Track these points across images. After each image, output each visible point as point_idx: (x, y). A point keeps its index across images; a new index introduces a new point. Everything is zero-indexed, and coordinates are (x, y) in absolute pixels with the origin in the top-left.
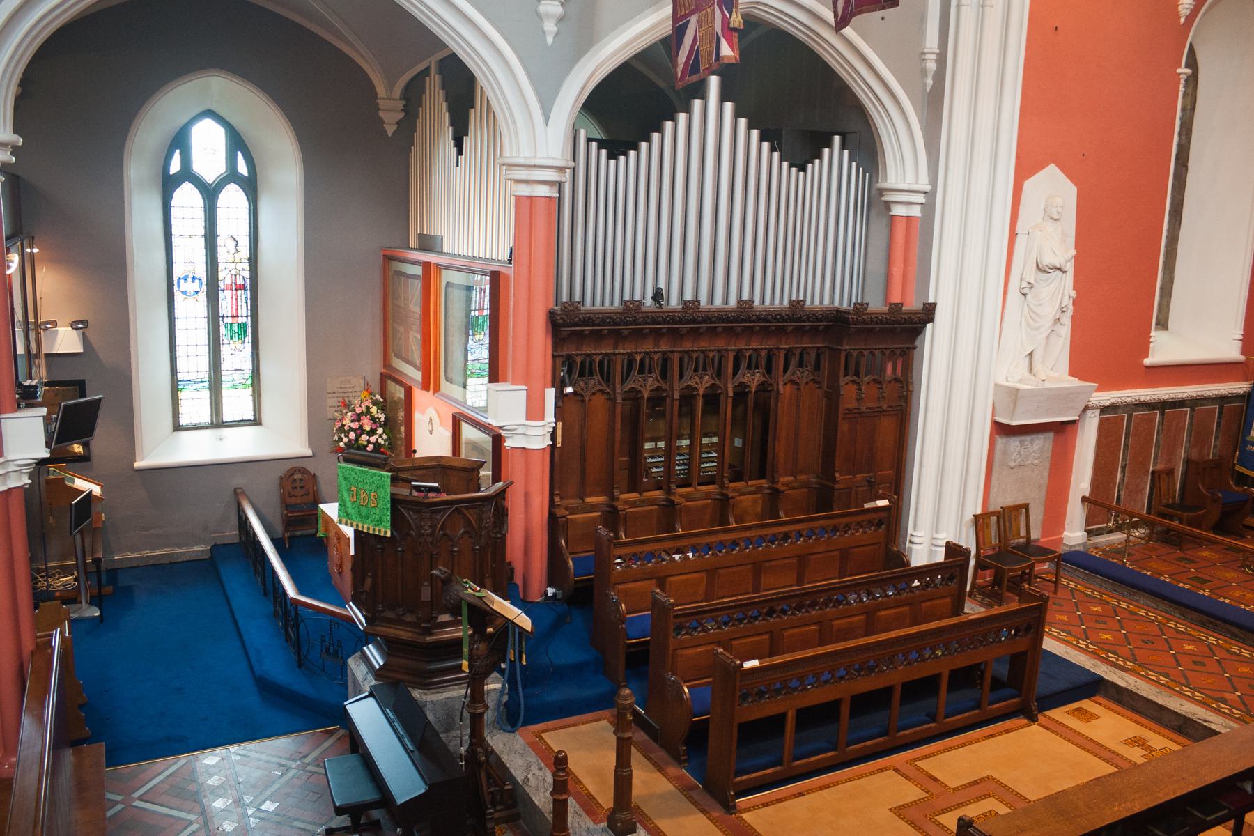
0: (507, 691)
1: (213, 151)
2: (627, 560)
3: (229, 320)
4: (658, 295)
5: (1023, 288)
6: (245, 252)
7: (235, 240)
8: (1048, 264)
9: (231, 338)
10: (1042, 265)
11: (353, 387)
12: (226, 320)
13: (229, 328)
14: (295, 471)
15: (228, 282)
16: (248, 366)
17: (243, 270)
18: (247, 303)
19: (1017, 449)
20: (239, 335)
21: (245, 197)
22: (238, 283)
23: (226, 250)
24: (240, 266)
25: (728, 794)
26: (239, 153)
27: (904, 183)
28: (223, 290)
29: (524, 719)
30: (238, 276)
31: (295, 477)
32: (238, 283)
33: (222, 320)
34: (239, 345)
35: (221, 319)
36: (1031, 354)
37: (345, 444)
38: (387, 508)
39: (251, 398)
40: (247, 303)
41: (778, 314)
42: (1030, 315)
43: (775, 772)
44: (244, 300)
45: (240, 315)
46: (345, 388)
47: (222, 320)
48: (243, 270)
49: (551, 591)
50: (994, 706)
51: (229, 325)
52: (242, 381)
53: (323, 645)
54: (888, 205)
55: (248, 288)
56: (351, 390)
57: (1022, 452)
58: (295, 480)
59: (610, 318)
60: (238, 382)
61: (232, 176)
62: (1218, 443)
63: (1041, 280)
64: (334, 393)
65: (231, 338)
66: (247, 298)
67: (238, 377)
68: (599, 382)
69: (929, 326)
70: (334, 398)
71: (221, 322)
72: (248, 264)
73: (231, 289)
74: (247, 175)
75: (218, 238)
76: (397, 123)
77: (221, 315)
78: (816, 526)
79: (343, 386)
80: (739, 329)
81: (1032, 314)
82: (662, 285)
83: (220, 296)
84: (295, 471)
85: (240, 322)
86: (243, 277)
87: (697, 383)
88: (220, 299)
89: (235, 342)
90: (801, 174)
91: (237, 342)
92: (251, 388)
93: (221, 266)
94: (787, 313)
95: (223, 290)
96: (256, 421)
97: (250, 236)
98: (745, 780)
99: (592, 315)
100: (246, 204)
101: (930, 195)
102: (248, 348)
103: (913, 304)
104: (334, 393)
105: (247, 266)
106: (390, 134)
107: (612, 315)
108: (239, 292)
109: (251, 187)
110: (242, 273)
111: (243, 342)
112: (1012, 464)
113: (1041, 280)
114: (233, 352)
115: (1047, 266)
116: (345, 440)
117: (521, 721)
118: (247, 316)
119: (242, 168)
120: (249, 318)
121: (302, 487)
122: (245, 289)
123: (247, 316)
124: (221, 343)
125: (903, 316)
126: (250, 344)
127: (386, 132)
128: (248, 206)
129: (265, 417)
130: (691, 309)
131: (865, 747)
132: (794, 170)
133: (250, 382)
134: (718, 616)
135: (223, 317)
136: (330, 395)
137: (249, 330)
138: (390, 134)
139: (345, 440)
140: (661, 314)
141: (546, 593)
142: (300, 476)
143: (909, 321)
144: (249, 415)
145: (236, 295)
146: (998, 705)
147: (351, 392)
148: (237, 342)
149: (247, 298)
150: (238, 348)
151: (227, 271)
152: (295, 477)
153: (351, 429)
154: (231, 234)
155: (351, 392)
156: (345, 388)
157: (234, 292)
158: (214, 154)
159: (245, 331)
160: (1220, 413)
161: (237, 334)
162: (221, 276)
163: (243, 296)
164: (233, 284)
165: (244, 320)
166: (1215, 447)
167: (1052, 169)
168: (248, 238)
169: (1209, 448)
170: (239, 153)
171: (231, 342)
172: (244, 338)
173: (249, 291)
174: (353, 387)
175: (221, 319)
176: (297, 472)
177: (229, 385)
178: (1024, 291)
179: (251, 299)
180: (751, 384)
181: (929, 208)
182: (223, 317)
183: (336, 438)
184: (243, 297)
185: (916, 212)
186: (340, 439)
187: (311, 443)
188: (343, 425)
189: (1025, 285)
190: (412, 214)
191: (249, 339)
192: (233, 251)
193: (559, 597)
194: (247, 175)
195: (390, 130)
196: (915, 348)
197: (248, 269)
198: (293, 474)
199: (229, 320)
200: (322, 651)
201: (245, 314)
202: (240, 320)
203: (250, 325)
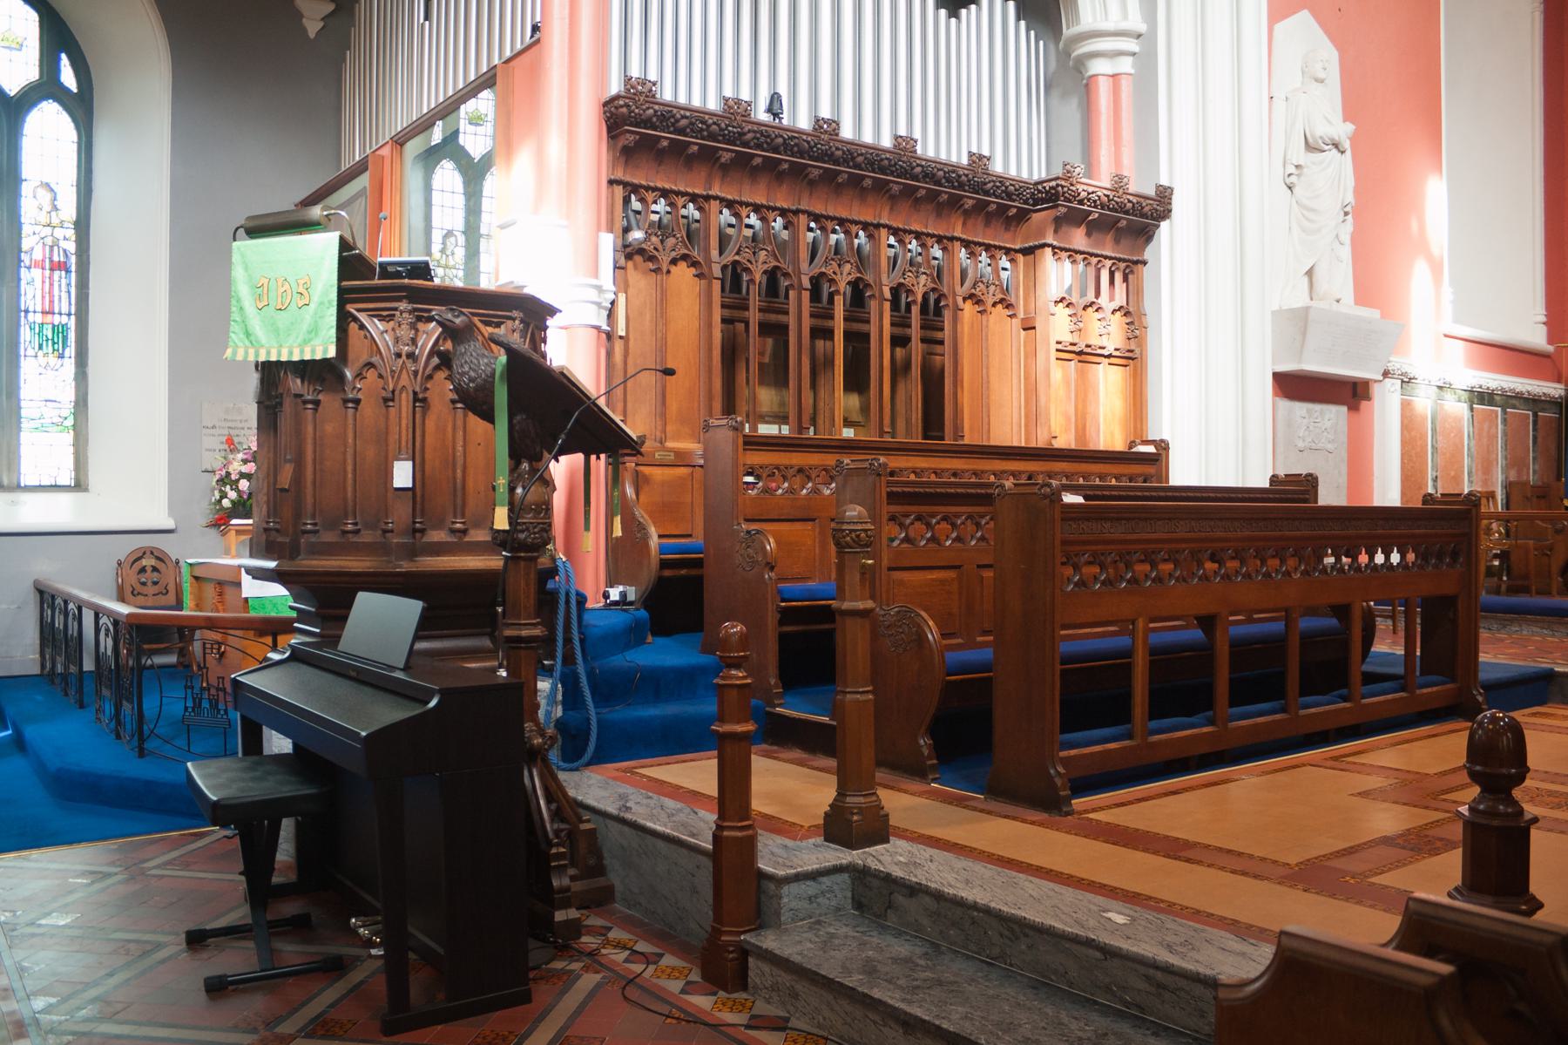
0: (560, 697)
1: (18, 47)
2: (764, 475)
3: (39, 318)
4: (774, 107)
5: (1289, 175)
6: (69, 210)
7: (52, 190)
8: (1322, 134)
9: (40, 347)
10: (1312, 136)
11: (246, 421)
12: (31, 316)
13: (37, 331)
14: (144, 553)
15: (38, 255)
16: (68, 395)
17: (65, 239)
18: (69, 292)
19: (1305, 421)
20: (54, 343)
21: (72, 125)
22: (56, 258)
23: (36, 203)
24: (59, 233)
25: (1052, 771)
26: (63, 56)
27: (1106, 20)
28: (29, 268)
29: (597, 748)
30: (56, 248)
31: (144, 562)
32: (56, 258)
33: (26, 317)
34: (53, 360)
35: (23, 314)
36: (1310, 273)
37: (232, 501)
38: (330, 302)
39: (71, 449)
40: (69, 292)
41: (954, 172)
42: (1303, 215)
43: (1124, 748)
44: (64, 288)
45: (56, 311)
46: (232, 421)
47: (26, 317)
48: (65, 239)
49: (615, 594)
50: (1425, 691)
51: (37, 326)
52: (57, 420)
53: (189, 695)
54: (1081, 62)
55: (73, 268)
56: (240, 426)
57: (1311, 428)
58: (143, 570)
59: (703, 122)
60: (50, 421)
61: (48, 87)
62: (1537, 467)
63: (1314, 163)
64: (214, 427)
65: (40, 347)
66: (69, 285)
67: (51, 413)
68: (683, 242)
69: (1164, 225)
70: (213, 435)
71: (22, 319)
72: (73, 231)
73: (43, 269)
74: (75, 91)
75: (24, 183)
76: (323, 19)
77: (23, 308)
78: (1057, 470)
79: (229, 418)
80: (896, 188)
81: (1305, 212)
82: (783, 89)
83: (22, 276)
84: (144, 553)
85: (56, 323)
86: (65, 251)
87: (834, 273)
88: (23, 283)
89: (46, 355)
90: (953, 20)
91: (51, 356)
92: (72, 432)
93: (26, 229)
94: (966, 172)
95: (29, 268)
96: (79, 485)
97: (78, 186)
98: (1075, 756)
99: (675, 111)
100: (73, 135)
101: (1145, 38)
102: (69, 365)
103: (1141, 185)
104: (214, 427)
105: (71, 233)
106: (312, 35)
107: (707, 117)
108: (57, 274)
109: (82, 108)
110: (63, 244)
111: (61, 356)
112: (1301, 444)
113: (1314, 163)
114: (43, 371)
115: (1321, 137)
116: (233, 495)
117: (587, 757)
118: (69, 315)
119: (68, 78)
120: (73, 317)
121: (155, 583)
122: (68, 271)
123: (69, 315)
124: (22, 353)
125: (1131, 198)
126: (73, 360)
127: (305, 30)
128: (76, 139)
129: (94, 477)
130: (826, 132)
131: (1256, 725)
132: (943, 12)
133: (70, 422)
134: (957, 515)
135: (27, 311)
136: (205, 431)
137: (72, 336)
138: (312, 35)
139: (233, 495)
140: (781, 132)
141: (606, 596)
142: (153, 562)
143: (1137, 210)
144: (66, 478)
145: (51, 278)
146: (1429, 690)
147: (243, 429)
148: (51, 356)
149: (69, 285)
150: (52, 364)
151: (37, 238)
152: (144, 562)
153: (243, 475)
154: (45, 180)
155: (243, 429)
156: (232, 421)
157: (47, 272)
158: (20, 50)
159: (65, 338)
160: (1535, 423)
161: (50, 342)
162: (25, 245)
163: (64, 281)
164: (47, 261)
165: (64, 319)
166: (1534, 471)
167: (1305, 15)
168: (74, 189)
169: (1528, 473)
170: (63, 56)
171: (40, 353)
172: (64, 350)
173: (73, 275)
174: (246, 421)
175: (23, 314)
176: (148, 553)
177: (37, 424)
178: (1289, 181)
179: (77, 287)
180: (915, 289)
181: (1146, 60)
182: (27, 311)
183: (217, 495)
184: (65, 285)
185: (1125, 65)
186: (224, 495)
187: (172, 509)
188: (228, 474)
189: (1292, 169)
190: (346, 127)
191: (71, 351)
192: (47, 207)
193: (631, 597)
194: (75, 91)
195: (313, 27)
196: (1145, 263)
197: (73, 238)
198: (139, 559)
199: (39, 318)
200: (186, 708)
201: (65, 310)
202: (57, 319)
203: (73, 328)
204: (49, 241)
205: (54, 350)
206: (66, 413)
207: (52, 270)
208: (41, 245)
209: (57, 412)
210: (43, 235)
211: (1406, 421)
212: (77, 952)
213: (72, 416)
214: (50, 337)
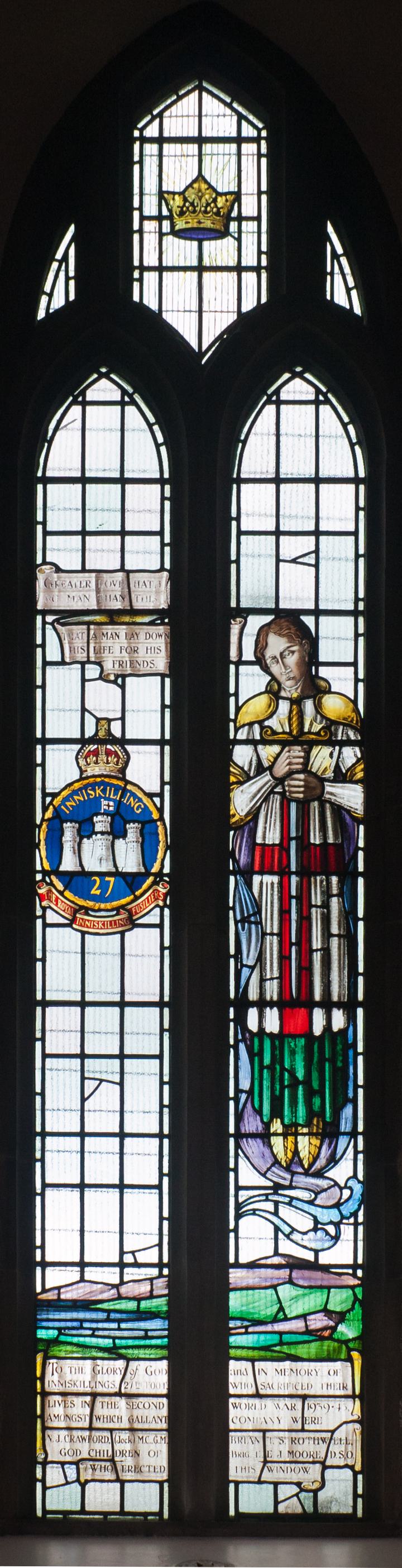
9: (277, 1112)
24: (322, 759)
50: (112, 1517)
52: (318, 1322)
65: (277, 1112)
66: (349, 915)
89: (290, 1131)
118: (349, 1007)
146: (115, 1517)
159: (341, 1077)
170: (329, 222)
171: (277, 1126)
204: (297, 784)
205: (311, 1114)
206: (339, 1300)
207: (305, 873)
208: (276, 801)
209: (315, 1300)
210: (281, 769)
211: (196, 1565)
212: (319, 768)
213: (358, 1310)
214: (300, 1074)
